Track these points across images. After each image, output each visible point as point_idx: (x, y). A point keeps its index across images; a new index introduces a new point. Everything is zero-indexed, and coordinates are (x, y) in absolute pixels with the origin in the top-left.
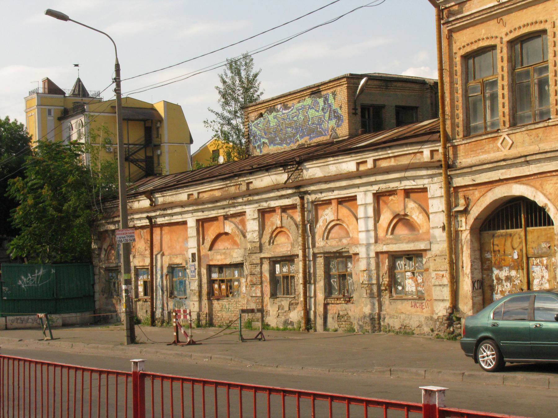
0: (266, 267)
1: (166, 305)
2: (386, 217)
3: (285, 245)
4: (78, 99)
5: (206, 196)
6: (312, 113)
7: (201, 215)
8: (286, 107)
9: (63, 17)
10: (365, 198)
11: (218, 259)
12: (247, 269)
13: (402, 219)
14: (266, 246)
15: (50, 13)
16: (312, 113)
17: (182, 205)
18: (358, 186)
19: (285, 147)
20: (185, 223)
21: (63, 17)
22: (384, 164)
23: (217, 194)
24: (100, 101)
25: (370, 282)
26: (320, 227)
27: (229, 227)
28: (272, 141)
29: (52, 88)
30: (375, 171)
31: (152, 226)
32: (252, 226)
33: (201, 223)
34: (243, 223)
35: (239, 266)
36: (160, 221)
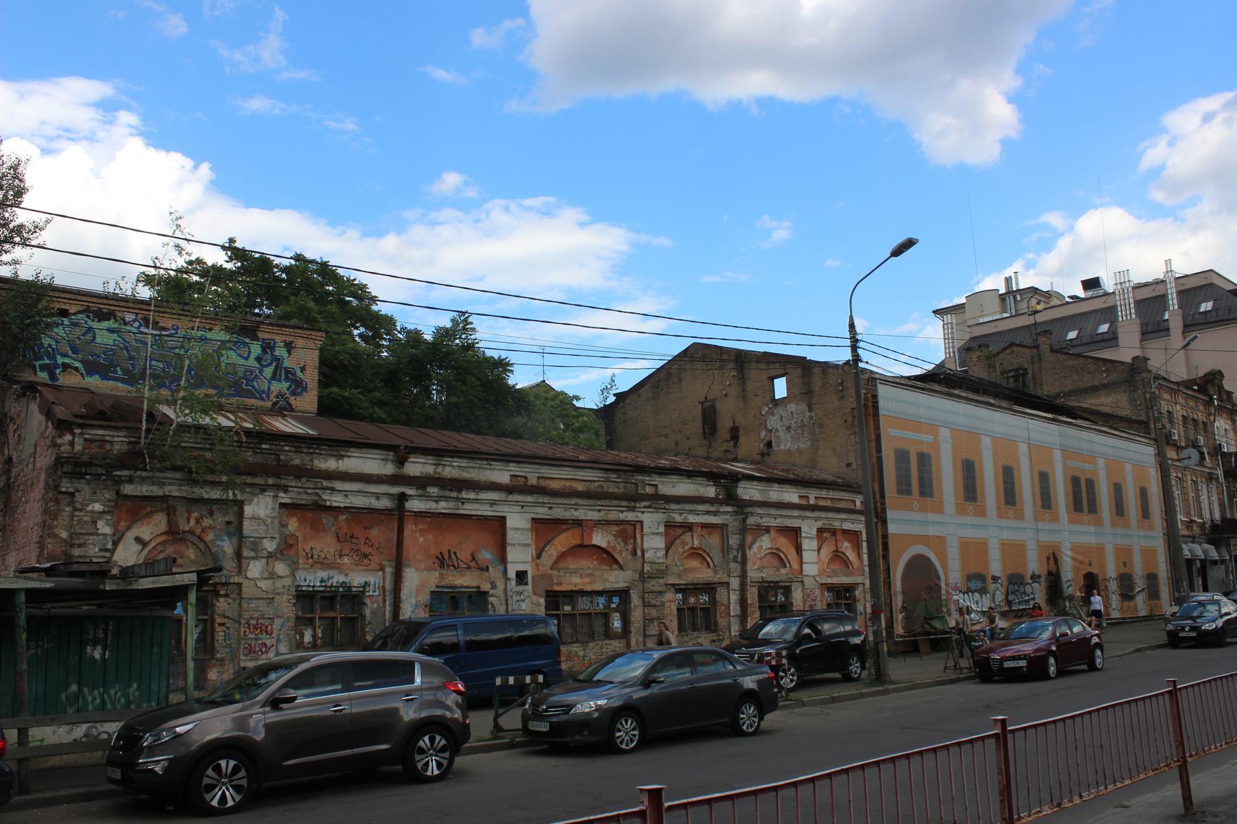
13: (838, 557)
22: (822, 503)
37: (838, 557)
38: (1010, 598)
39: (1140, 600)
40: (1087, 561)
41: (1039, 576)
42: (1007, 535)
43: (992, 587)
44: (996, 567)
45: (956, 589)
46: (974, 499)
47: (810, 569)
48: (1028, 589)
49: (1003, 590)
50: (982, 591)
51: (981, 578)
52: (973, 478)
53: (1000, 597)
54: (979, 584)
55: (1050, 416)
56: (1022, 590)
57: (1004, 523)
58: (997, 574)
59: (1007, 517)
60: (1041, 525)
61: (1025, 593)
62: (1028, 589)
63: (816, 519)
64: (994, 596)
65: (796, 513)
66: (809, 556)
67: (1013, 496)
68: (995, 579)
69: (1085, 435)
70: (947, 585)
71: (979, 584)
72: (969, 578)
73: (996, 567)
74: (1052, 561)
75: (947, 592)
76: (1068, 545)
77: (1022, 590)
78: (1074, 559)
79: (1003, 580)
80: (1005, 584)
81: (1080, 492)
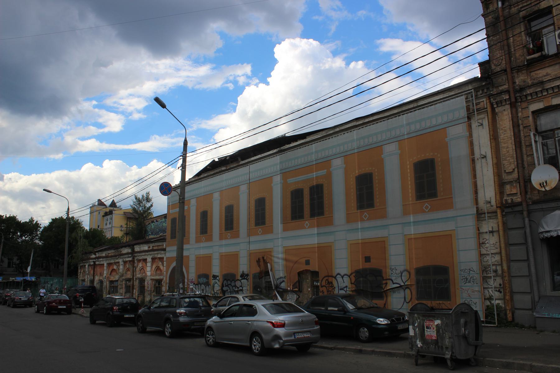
0: (124, 282)
1: (534, 283)
2: (154, 267)
3: (129, 275)
4: (112, 208)
5: (110, 255)
6: (164, 224)
7: (108, 262)
8: (157, 221)
9: (163, 106)
10: (149, 259)
11: (112, 278)
12: (119, 282)
13: (158, 268)
14: (125, 275)
15: (44, 190)
16: (164, 224)
17: (103, 257)
18: (147, 255)
19: (156, 236)
20: (103, 264)
21: (163, 106)
22: (155, 248)
23: (113, 254)
24: (121, 209)
25: (477, 277)
26: (138, 269)
27: (115, 267)
28: (152, 234)
29: (100, 203)
30: (153, 250)
31: (95, 265)
32: (121, 267)
33: (109, 265)
34: (119, 266)
35: (117, 281)
36: (97, 263)
37: (158, 268)
38: (225, 289)
39: (136, 292)
40: (303, 260)
41: (247, 275)
42: (224, 250)
43: (212, 282)
44: (216, 270)
45: (192, 282)
46: (232, 228)
47: (149, 274)
48: (238, 284)
49: (220, 283)
50: (207, 284)
51: (206, 276)
52: (206, 221)
53: (217, 288)
54: (205, 280)
55: (275, 151)
56: (233, 284)
57: (224, 242)
58: (215, 274)
59: (226, 238)
60: (253, 239)
61: (235, 286)
62: (238, 284)
63: (151, 255)
64: (213, 287)
65: (144, 254)
66: (148, 269)
67: (206, 228)
68: (215, 277)
69: (253, 167)
70: (188, 280)
71: (205, 280)
72: (199, 276)
73: (216, 270)
74: (262, 263)
75: (187, 283)
76: (280, 249)
77: (233, 284)
78: (286, 260)
79: (220, 278)
80: (221, 280)
81: (175, 226)
